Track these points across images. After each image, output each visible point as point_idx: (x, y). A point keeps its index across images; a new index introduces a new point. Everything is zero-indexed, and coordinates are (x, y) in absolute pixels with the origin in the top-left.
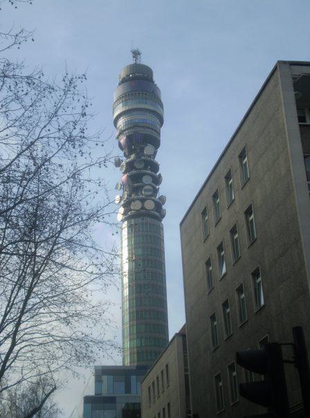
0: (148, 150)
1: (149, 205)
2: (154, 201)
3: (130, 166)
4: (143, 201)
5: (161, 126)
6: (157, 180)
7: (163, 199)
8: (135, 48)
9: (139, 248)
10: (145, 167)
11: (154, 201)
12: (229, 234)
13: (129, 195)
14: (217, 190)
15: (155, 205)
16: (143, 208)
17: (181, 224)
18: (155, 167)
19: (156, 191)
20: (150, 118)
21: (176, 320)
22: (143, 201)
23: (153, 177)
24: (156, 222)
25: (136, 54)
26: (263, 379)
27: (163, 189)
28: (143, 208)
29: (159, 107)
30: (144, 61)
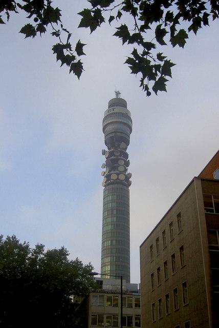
0: (123, 145)
1: (122, 177)
2: (125, 175)
3: (111, 154)
4: (118, 174)
5: (131, 132)
6: (127, 164)
7: (130, 175)
8: (117, 90)
9: (115, 195)
10: (120, 156)
11: (125, 175)
13: (110, 171)
14: (79, 14)
15: (126, 178)
16: (118, 178)
18: (126, 156)
19: (126, 170)
20: (126, 128)
21: (135, 277)
22: (118, 174)
23: (125, 161)
24: (125, 187)
25: (118, 93)
27: (130, 170)
28: (118, 178)
29: (95, 276)
30: (122, 96)
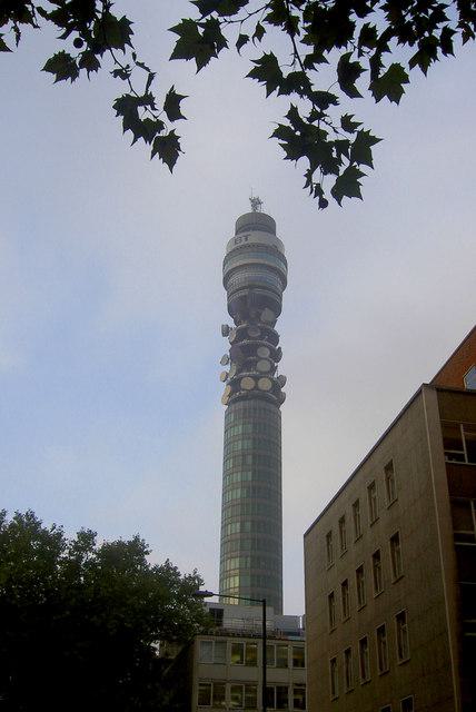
0: (267, 314)
1: (265, 384)
2: (271, 379)
3: (242, 334)
4: (256, 379)
5: (284, 287)
6: (276, 355)
7: (282, 381)
8: (255, 196)
9: (249, 423)
10: (261, 338)
11: (271, 379)
12: (351, 507)
13: (239, 371)
15: (273, 386)
16: (256, 387)
17: (305, 536)
18: (275, 338)
19: (274, 369)
20: (273, 279)
21: (294, 601)
22: (256, 379)
23: (272, 350)
24: (272, 407)
25: (256, 203)
26: (250, 479)
27: (282, 368)
28: (256, 387)
30: (264, 209)
